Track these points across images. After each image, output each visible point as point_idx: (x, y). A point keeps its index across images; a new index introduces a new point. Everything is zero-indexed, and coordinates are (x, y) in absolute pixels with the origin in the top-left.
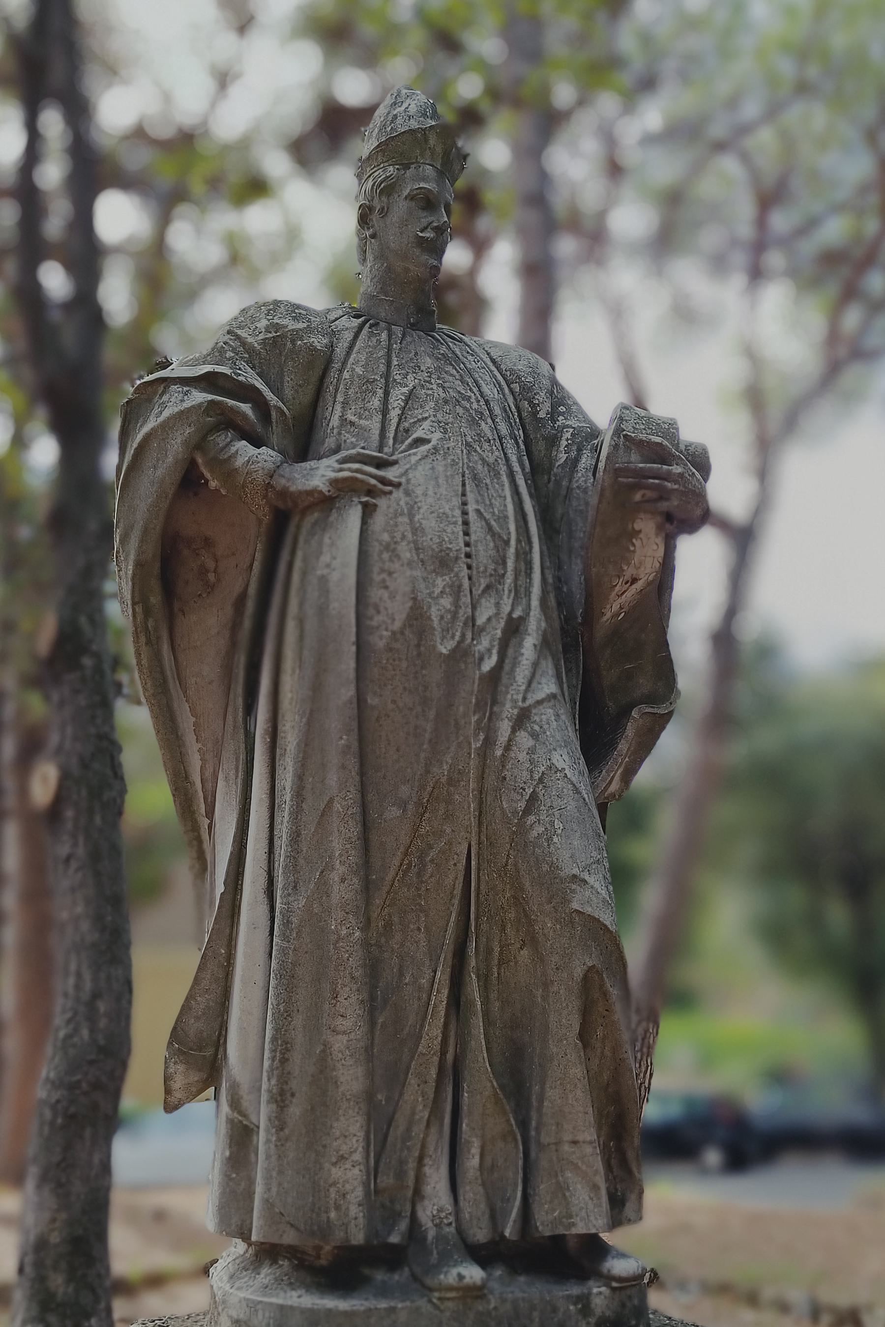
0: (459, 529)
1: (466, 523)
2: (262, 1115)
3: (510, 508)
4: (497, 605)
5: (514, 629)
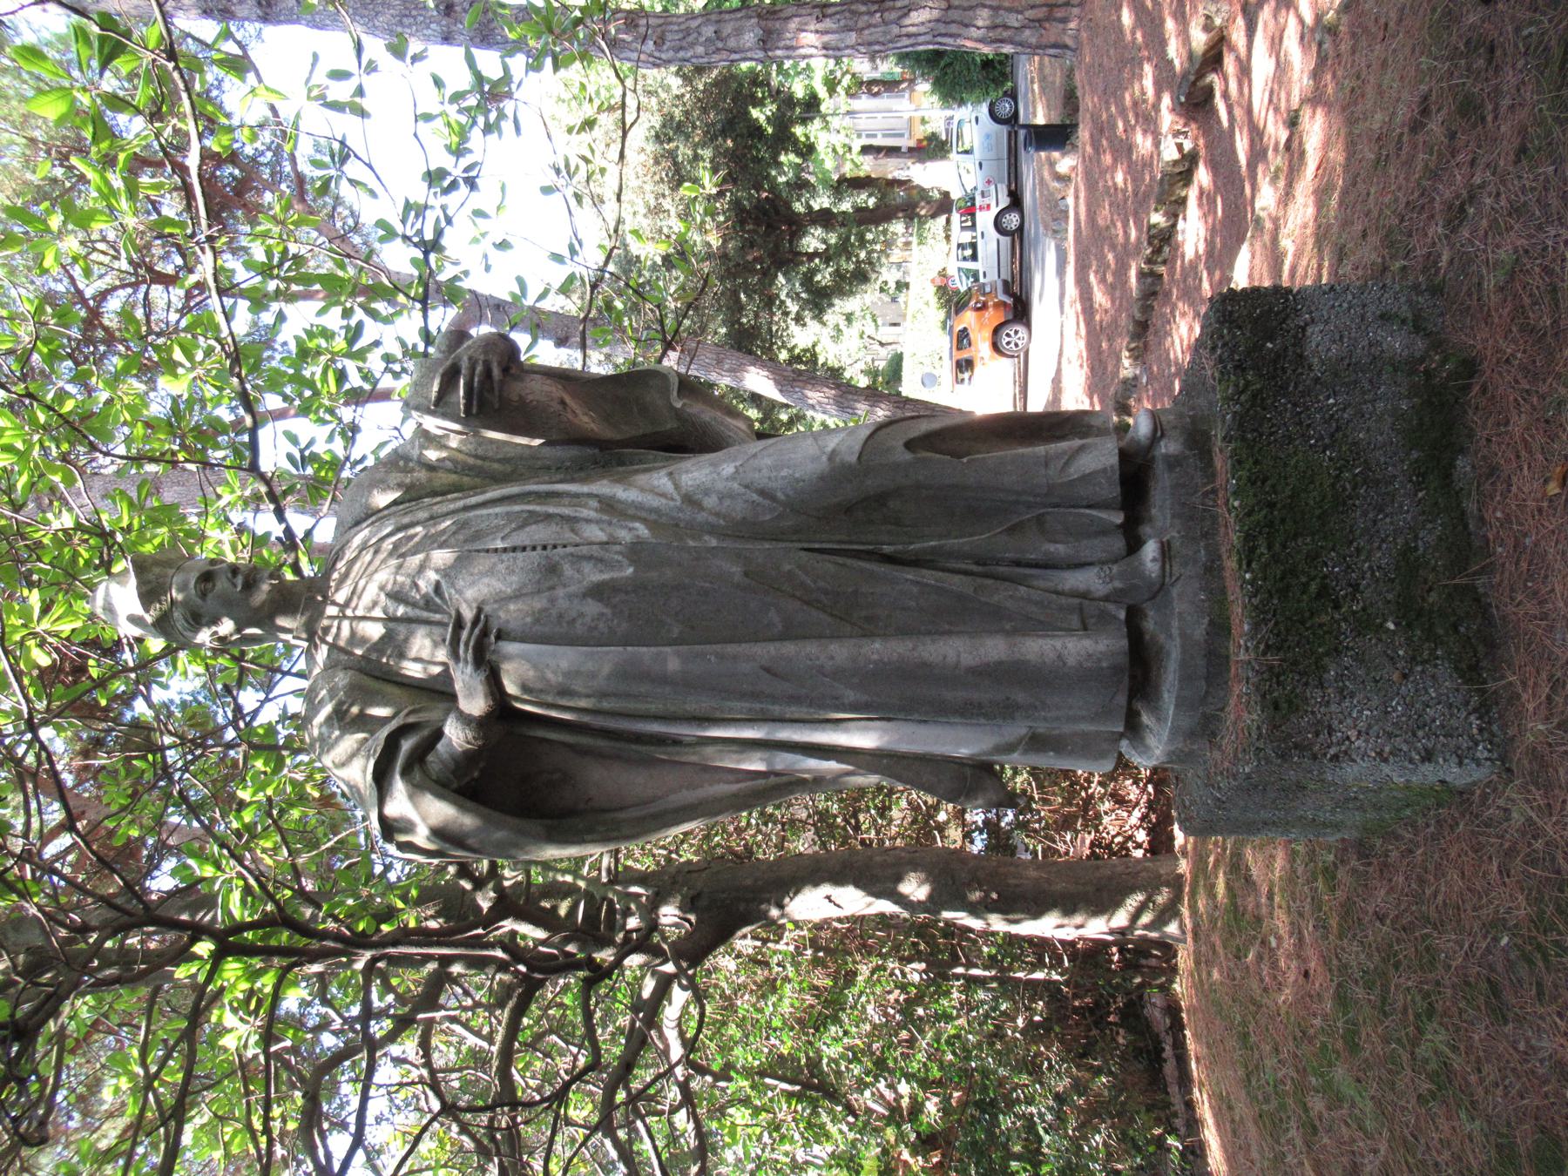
0: (520, 555)
1: (514, 549)
2: (1017, 730)
3: (498, 510)
4: (588, 521)
5: (609, 506)
